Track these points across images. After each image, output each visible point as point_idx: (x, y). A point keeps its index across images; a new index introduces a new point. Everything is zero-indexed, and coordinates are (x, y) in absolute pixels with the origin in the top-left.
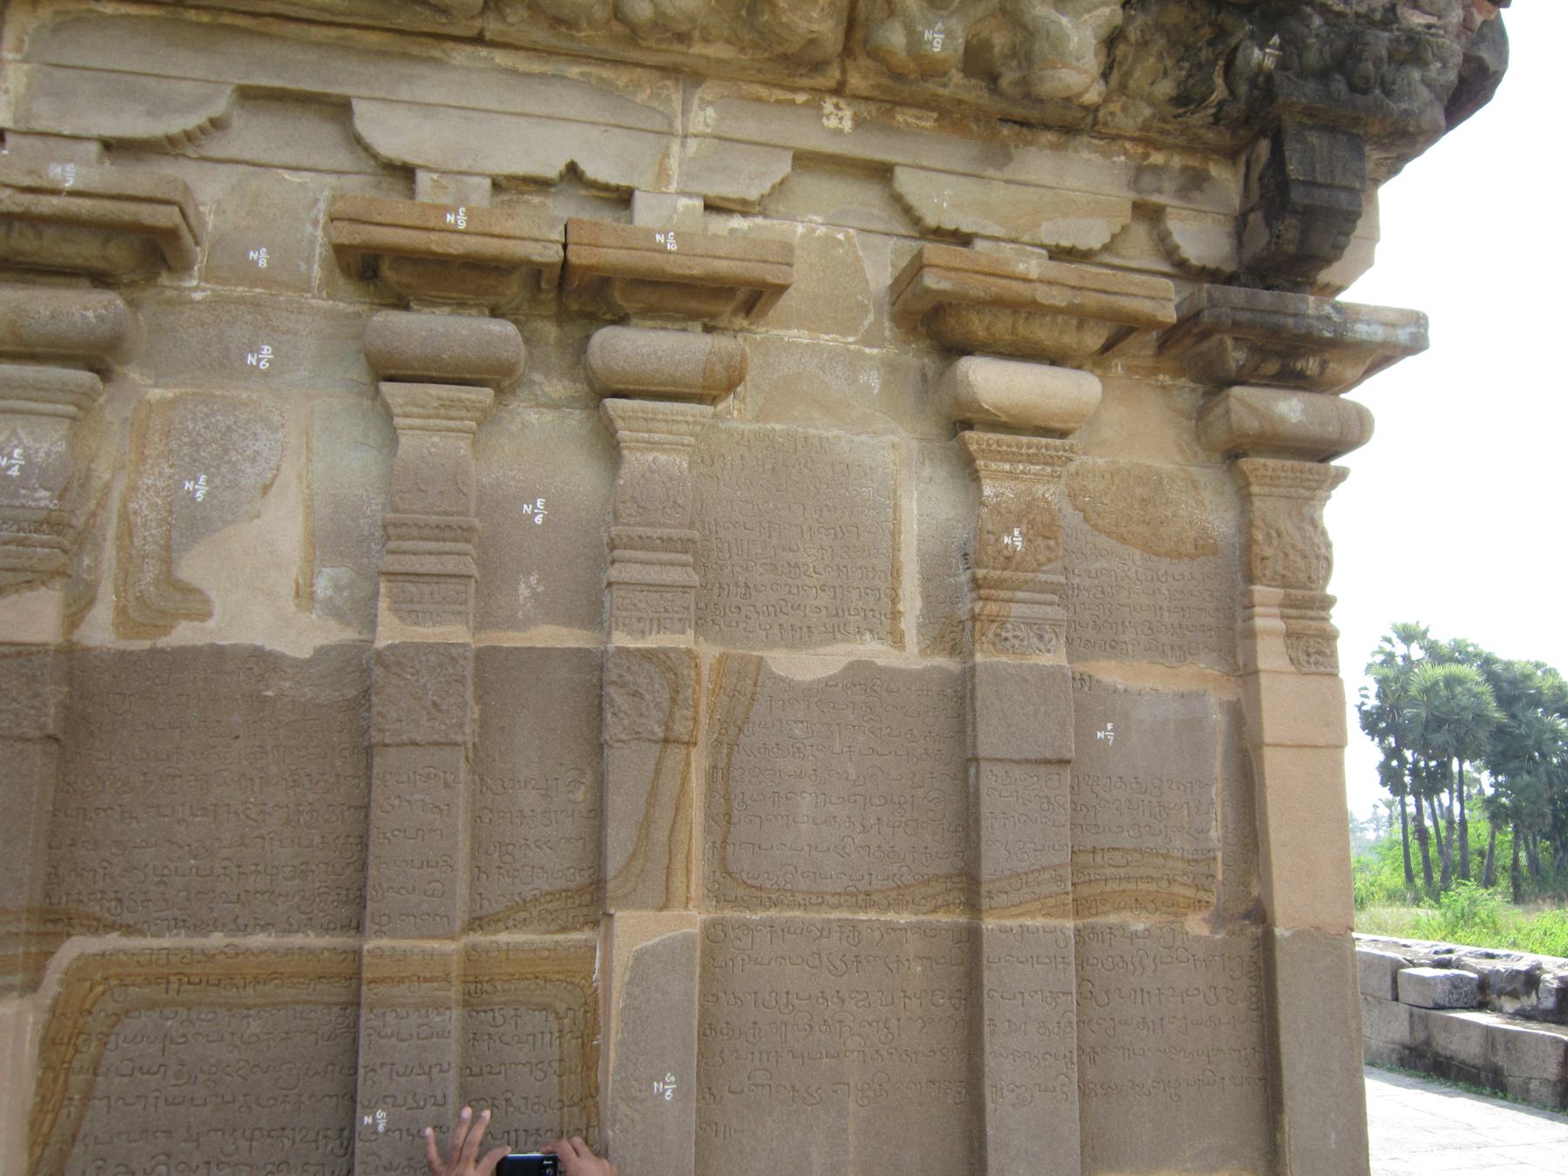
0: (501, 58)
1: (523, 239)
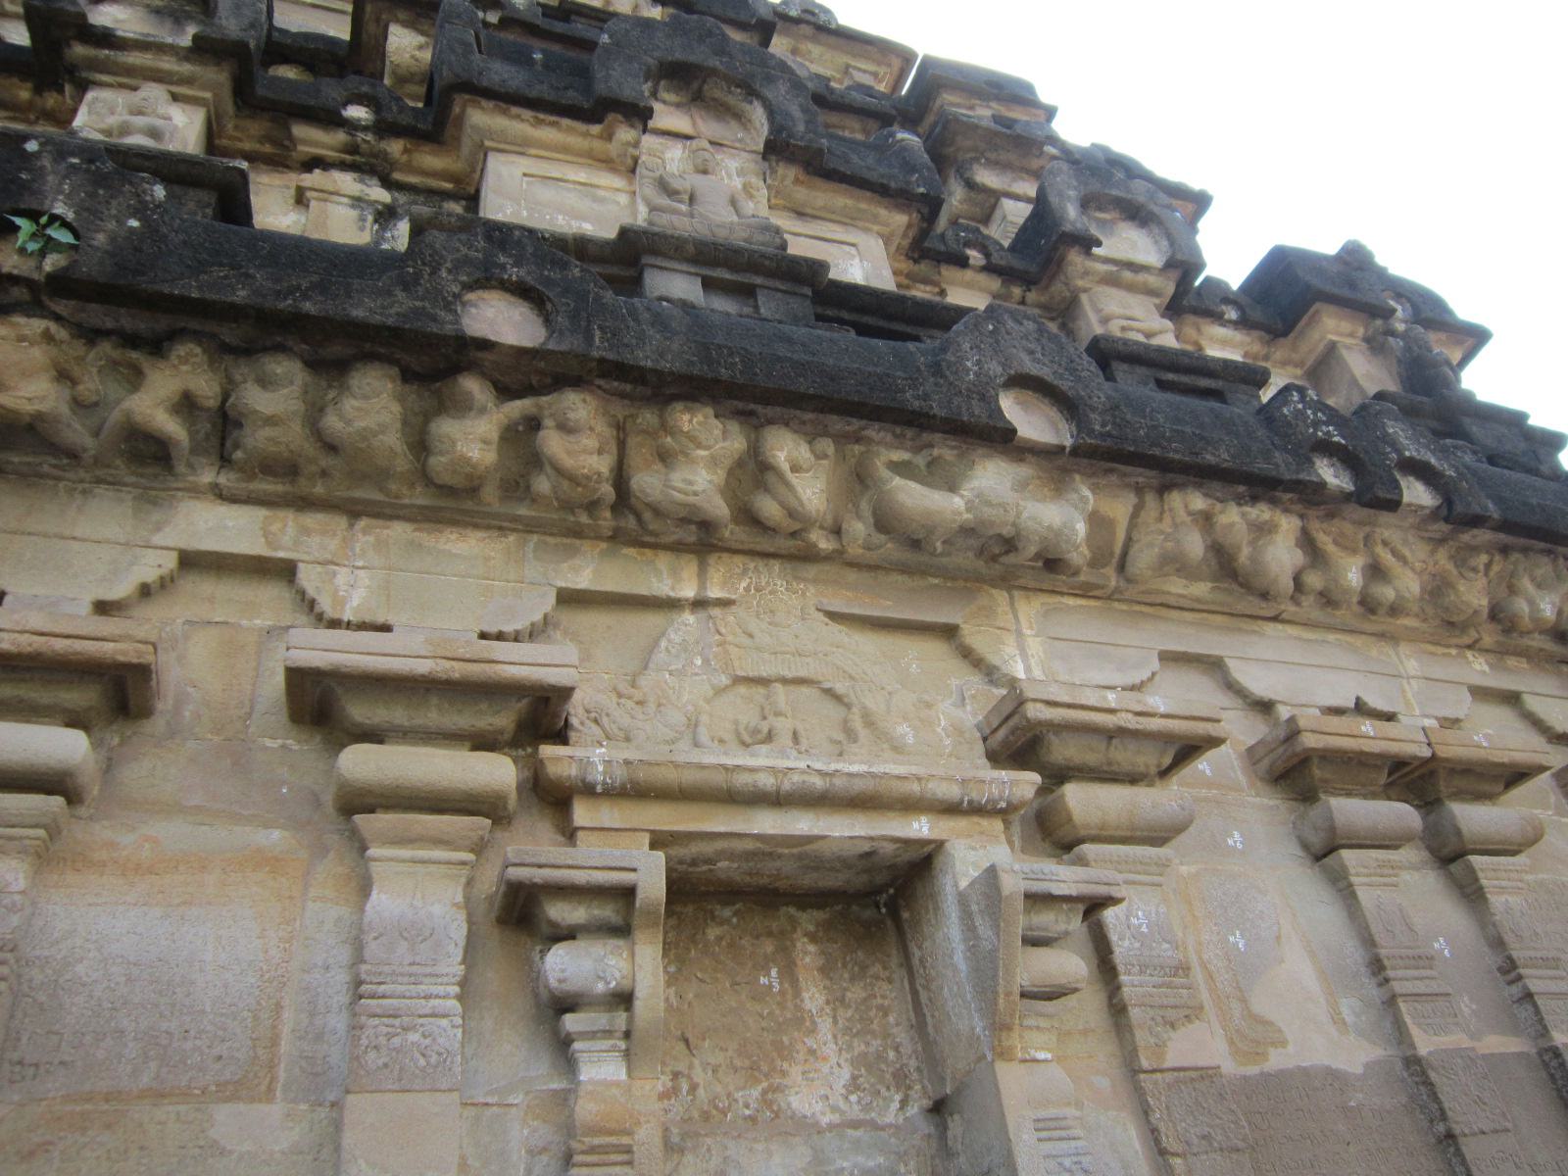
0: (1291, 630)
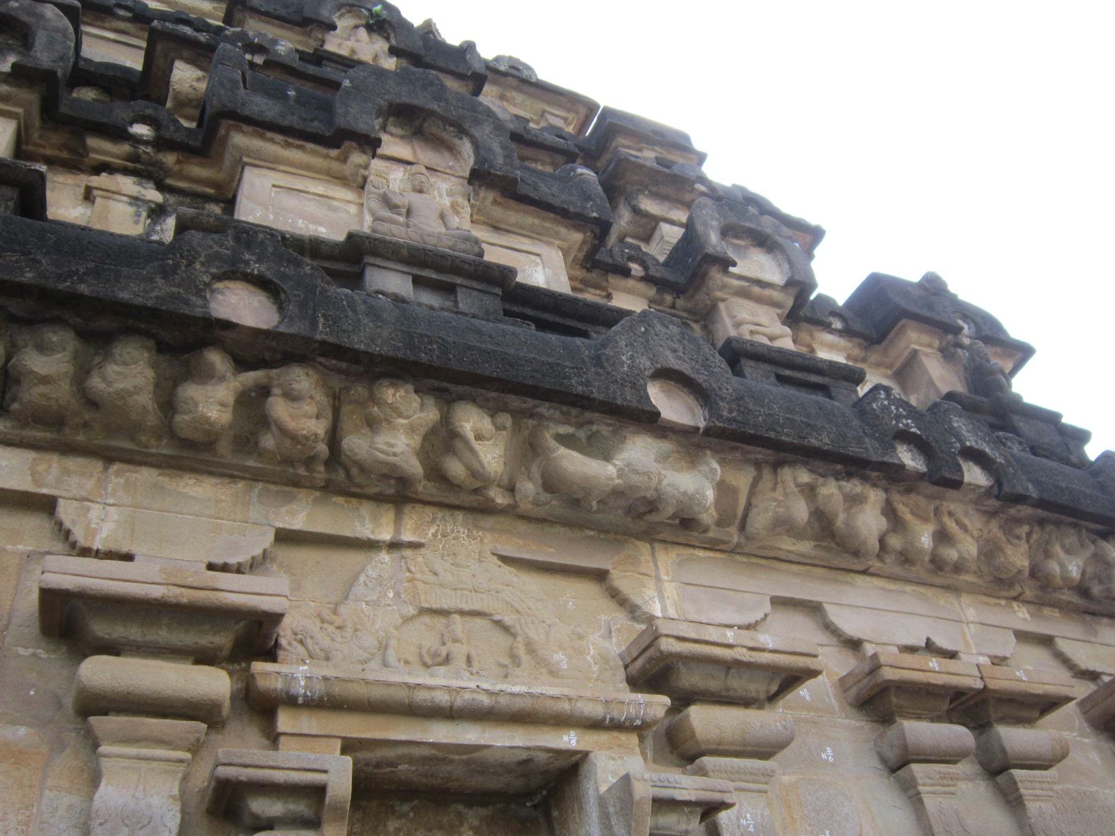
1: (963, 675)
